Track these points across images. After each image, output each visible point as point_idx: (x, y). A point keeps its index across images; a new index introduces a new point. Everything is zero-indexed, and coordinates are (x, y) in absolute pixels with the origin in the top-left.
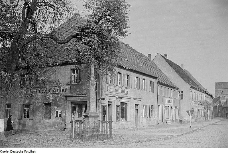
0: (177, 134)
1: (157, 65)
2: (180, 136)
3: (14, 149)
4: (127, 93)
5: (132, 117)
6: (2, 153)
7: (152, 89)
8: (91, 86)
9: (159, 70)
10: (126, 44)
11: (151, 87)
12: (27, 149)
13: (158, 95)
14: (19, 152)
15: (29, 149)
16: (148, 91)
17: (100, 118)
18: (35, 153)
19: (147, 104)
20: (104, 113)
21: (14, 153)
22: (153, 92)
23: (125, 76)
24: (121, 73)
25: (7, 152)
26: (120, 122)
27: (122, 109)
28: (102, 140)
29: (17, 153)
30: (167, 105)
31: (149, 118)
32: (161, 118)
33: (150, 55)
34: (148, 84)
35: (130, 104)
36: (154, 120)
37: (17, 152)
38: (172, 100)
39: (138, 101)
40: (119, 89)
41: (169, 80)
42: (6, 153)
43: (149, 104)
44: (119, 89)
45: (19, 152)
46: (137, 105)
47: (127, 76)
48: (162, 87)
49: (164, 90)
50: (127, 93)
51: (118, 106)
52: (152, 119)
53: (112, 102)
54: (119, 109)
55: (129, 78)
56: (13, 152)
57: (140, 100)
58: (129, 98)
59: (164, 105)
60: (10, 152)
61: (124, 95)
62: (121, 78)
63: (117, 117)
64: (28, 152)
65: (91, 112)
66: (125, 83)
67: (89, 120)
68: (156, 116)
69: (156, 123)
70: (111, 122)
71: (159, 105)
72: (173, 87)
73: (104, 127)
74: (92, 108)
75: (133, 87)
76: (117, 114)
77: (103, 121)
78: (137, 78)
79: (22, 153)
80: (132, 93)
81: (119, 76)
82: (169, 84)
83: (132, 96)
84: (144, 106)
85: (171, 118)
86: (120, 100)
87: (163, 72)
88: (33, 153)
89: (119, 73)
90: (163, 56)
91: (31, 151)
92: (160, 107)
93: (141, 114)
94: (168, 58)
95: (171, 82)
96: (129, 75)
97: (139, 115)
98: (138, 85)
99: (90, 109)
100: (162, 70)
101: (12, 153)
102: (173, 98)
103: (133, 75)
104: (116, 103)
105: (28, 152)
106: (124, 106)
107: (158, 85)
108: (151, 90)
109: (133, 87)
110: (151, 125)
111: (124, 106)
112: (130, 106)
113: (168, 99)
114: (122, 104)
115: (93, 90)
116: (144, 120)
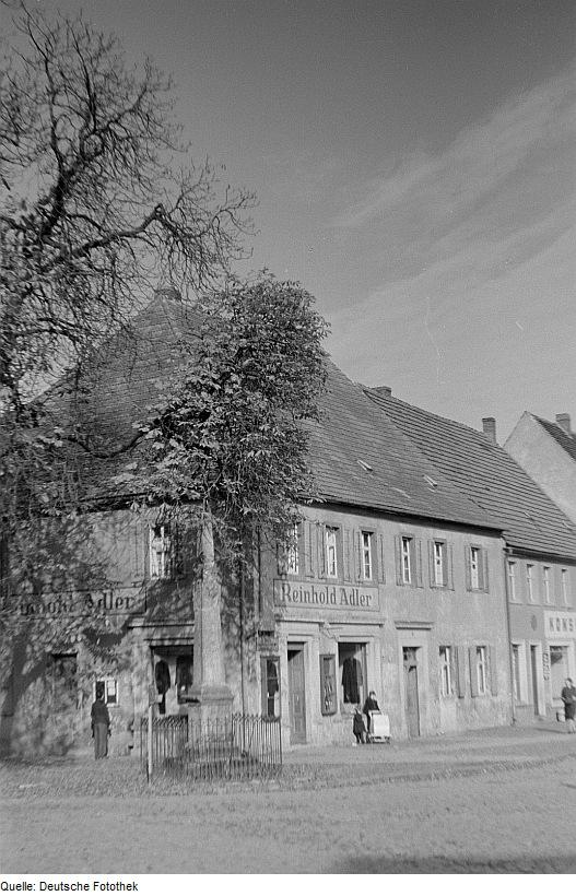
1: (522, 464)
3: (55, 879)
5: (390, 696)
8: (206, 600)
10: (372, 383)
11: (475, 572)
12: (103, 878)
13: (515, 598)
14: (74, 887)
15: (113, 879)
20: (273, 686)
22: (484, 589)
23: (356, 537)
24: (336, 529)
25: (28, 887)
30: (560, 639)
31: (467, 700)
32: (526, 697)
33: (489, 422)
36: (493, 705)
37: (67, 888)
39: (416, 632)
40: (331, 591)
43: (466, 643)
44: (331, 591)
45: (74, 887)
46: (415, 649)
51: (326, 659)
53: (303, 643)
56: (50, 887)
58: (375, 622)
59: (544, 640)
60: (37, 887)
61: (354, 613)
62: (340, 548)
65: (210, 684)
67: (200, 712)
68: (503, 691)
69: (503, 720)
73: (259, 739)
75: (390, 580)
83: (388, 616)
87: (550, 493)
90: (552, 420)
91: (119, 886)
92: (523, 651)
103: (389, 530)
105: (107, 887)
106: (358, 656)
107: (511, 559)
110: (478, 725)
111: (358, 656)
114: (347, 649)
116: (443, 708)
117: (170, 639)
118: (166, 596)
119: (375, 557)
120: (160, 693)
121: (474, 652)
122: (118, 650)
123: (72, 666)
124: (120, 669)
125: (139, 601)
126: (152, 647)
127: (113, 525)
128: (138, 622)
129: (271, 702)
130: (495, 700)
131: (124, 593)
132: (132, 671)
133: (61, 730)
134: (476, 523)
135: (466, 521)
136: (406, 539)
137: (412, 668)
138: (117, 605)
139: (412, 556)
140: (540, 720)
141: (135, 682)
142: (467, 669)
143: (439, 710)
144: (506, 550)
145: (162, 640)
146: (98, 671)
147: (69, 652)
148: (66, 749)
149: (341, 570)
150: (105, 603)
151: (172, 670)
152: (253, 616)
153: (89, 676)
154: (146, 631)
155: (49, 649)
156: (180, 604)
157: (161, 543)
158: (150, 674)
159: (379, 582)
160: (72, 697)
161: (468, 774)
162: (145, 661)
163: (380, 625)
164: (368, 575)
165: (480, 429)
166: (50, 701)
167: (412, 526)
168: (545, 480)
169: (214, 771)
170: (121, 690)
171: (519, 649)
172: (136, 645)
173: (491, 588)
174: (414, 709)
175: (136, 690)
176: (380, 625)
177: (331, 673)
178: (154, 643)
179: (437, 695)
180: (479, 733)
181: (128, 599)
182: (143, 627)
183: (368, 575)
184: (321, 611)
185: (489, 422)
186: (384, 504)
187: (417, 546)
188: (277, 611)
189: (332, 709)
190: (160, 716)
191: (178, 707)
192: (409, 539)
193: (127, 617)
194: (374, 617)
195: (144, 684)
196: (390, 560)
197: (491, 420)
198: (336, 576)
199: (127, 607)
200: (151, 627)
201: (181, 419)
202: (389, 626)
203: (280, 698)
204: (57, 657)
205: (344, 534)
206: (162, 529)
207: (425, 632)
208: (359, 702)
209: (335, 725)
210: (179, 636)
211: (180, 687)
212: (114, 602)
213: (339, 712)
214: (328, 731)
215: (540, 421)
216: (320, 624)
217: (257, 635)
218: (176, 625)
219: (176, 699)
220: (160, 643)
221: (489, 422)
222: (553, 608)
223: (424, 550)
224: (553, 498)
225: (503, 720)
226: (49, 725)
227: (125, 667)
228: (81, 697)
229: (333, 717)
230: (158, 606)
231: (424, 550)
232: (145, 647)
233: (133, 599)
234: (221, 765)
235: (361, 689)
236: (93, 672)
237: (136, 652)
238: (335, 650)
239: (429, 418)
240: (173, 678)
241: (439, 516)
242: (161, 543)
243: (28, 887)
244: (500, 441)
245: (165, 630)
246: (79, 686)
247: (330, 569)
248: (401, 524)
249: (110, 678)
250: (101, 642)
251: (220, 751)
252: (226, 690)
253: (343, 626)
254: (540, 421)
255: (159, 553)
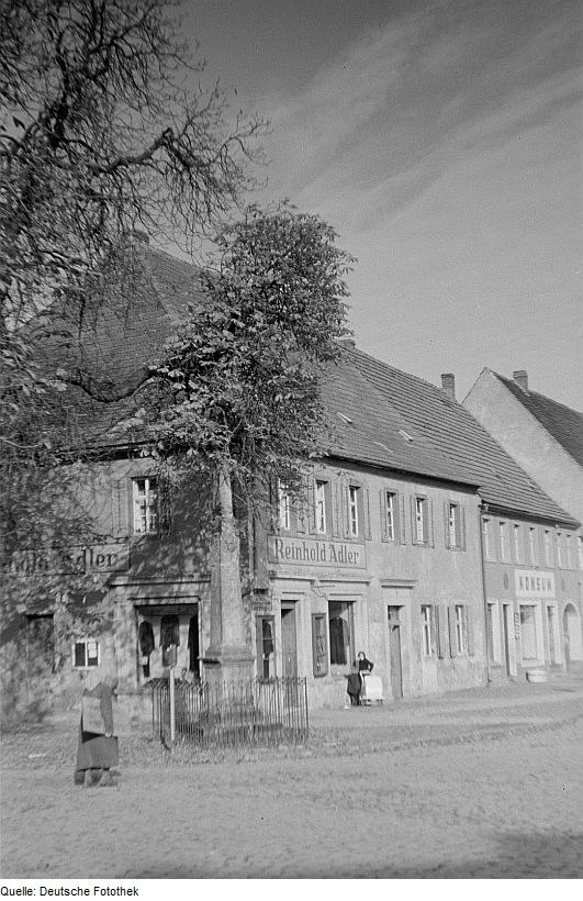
0: (547, 720)
1: (481, 421)
2: (558, 725)
3: (55, 884)
4: (353, 560)
6: (9, 898)
7: (458, 536)
9: (490, 447)
11: (453, 528)
12: (103, 883)
13: (488, 557)
14: (74, 892)
16: (440, 545)
17: (255, 671)
18: (133, 898)
19: (437, 603)
20: (268, 647)
21: (54, 898)
22: (461, 547)
24: (325, 483)
25: (29, 892)
26: (329, 678)
27: (337, 626)
28: (273, 742)
29: (65, 898)
31: (447, 660)
32: (499, 658)
33: (448, 378)
34: (438, 517)
35: (365, 604)
36: (470, 664)
38: (550, 576)
39: (399, 590)
40: (321, 547)
41: (535, 489)
42: (22, 898)
43: (445, 601)
44: (321, 547)
45: (74, 892)
46: (397, 608)
47: (352, 490)
48: (502, 523)
49: (512, 534)
50: (353, 560)
51: (317, 618)
52: (461, 663)
53: (295, 601)
54: (325, 627)
55: (360, 501)
56: (50, 892)
57: (410, 588)
59: (515, 600)
60: (37, 892)
61: (343, 571)
62: (328, 504)
63: (317, 658)
64: (107, 892)
66: (345, 523)
67: (220, 674)
68: (480, 651)
69: (479, 682)
70: (292, 681)
71: (489, 602)
72: (551, 522)
73: (270, 701)
74: (231, 629)
75: (376, 536)
76: (317, 648)
77: (265, 678)
78: (393, 494)
79: (84, 898)
80: (373, 560)
81: (320, 494)
82: (533, 510)
83: (375, 573)
84: (423, 610)
85: (546, 654)
86: (328, 594)
87: (511, 451)
88: (127, 898)
89: (320, 483)
90: (510, 377)
91: (120, 891)
92: (496, 611)
93: (415, 642)
94: (534, 386)
95: (545, 497)
96: (357, 488)
97: (406, 647)
98: (397, 527)
99: (221, 637)
100: (503, 444)
101: (47, 897)
102: (556, 569)
103: (375, 484)
104: (311, 604)
105: (107, 892)
106: (344, 615)
107: (485, 516)
108: (453, 543)
109: (376, 536)
110: (456, 687)
111: (344, 615)
112: (365, 612)
113: (530, 574)
114: (335, 606)
115: (228, 565)
116: (424, 667)
117: (155, 598)
118: (152, 551)
119: (362, 512)
120: (144, 655)
121: (453, 611)
122: (102, 608)
123: (48, 626)
124: (101, 630)
125: (122, 558)
126: (136, 607)
127: (92, 479)
128: (121, 580)
129: (266, 663)
130: (472, 660)
131: (106, 550)
132: (114, 632)
133: (35, 695)
134: (455, 479)
135: (446, 476)
136: (391, 494)
137: (396, 627)
138: (98, 562)
139: (396, 512)
140: (512, 680)
141: (118, 644)
142: (447, 628)
143: (421, 671)
144: (482, 507)
145: (147, 599)
146: (78, 631)
147: (45, 612)
148: (42, 715)
149: (330, 525)
150: (85, 561)
151: (157, 630)
152: (248, 573)
153: (68, 637)
154: (130, 590)
155: (22, 609)
156: (167, 561)
157: (148, 496)
158: (134, 635)
159: (366, 538)
160: (47, 660)
161: (497, 737)
162: (129, 623)
163: (367, 583)
164: (354, 531)
165: (438, 384)
166: (23, 666)
167: (395, 481)
168: (505, 438)
169: (237, 737)
170: (103, 652)
171: (508, 608)
172: (119, 604)
173: (436, 544)
174: (397, 670)
175: (120, 652)
176: (367, 583)
177: (321, 633)
178: (138, 603)
179: (419, 656)
180: (463, 693)
181: (110, 556)
182: (126, 585)
183: (354, 531)
184: (311, 568)
185: (448, 378)
186: (371, 458)
187: (401, 502)
188: (270, 567)
189: (323, 670)
190: (144, 680)
191: (162, 670)
192: (393, 494)
193: (108, 575)
194: (361, 575)
195: (127, 647)
196: (375, 516)
197: (450, 376)
198: (325, 532)
199: (109, 564)
200: (136, 585)
201: (204, 359)
202: (375, 583)
203: (274, 659)
204: (31, 618)
205: (333, 489)
206: (147, 482)
207: (408, 590)
208: (345, 663)
209: (327, 688)
210: (166, 595)
211: (164, 649)
212: (94, 560)
213: (330, 673)
214: (324, 693)
215: (500, 378)
216: (312, 581)
217: (252, 594)
218: (165, 583)
219: (161, 661)
220: (144, 603)
221: (448, 378)
222: (522, 567)
223: (407, 506)
224: (512, 454)
225: (479, 682)
226: (23, 689)
227: (107, 627)
228: (57, 660)
229: (324, 679)
230: (143, 564)
231: (407, 506)
232: (129, 607)
233: (116, 555)
234: (245, 729)
235: (348, 649)
236: (72, 633)
237: (118, 612)
238: (325, 609)
239: (394, 373)
240: (157, 639)
241: (401, 466)
242: (148, 496)
243: (29, 892)
244: (459, 398)
245: (150, 589)
246: (57, 648)
247: (319, 525)
248: (386, 479)
249: (92, 640)
250: (81, 603)
251: (242, 715)
252: (247, 651)
253: (336, 584)
254: (500, 378)
255: (144, 507)
